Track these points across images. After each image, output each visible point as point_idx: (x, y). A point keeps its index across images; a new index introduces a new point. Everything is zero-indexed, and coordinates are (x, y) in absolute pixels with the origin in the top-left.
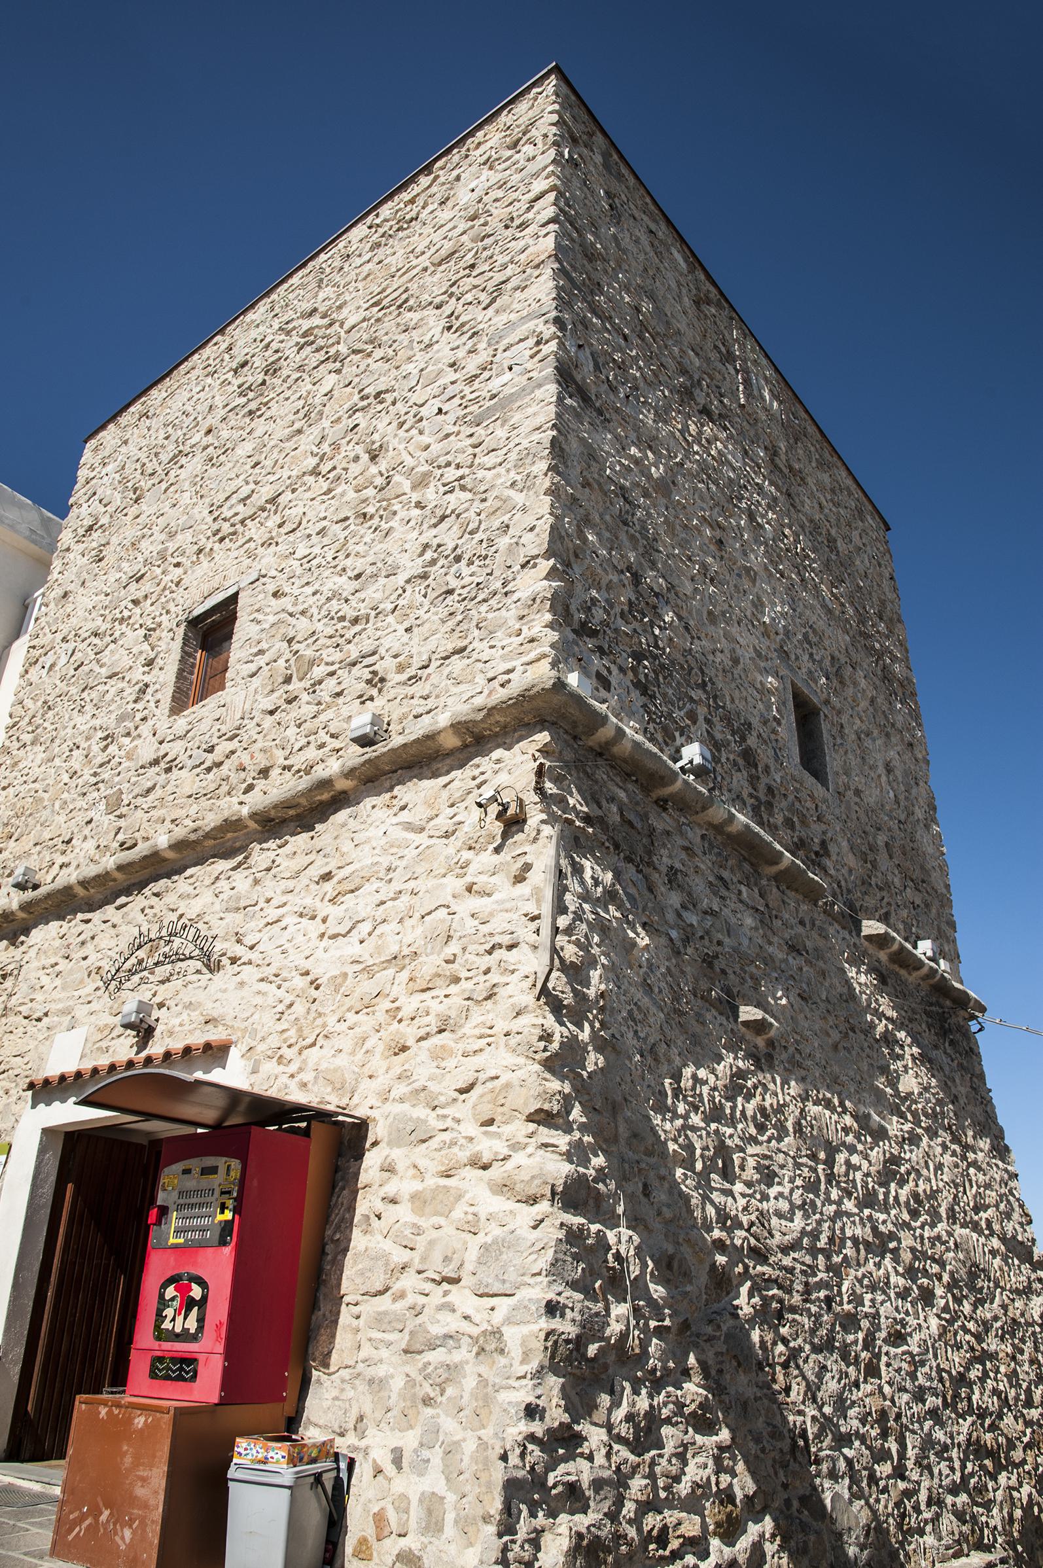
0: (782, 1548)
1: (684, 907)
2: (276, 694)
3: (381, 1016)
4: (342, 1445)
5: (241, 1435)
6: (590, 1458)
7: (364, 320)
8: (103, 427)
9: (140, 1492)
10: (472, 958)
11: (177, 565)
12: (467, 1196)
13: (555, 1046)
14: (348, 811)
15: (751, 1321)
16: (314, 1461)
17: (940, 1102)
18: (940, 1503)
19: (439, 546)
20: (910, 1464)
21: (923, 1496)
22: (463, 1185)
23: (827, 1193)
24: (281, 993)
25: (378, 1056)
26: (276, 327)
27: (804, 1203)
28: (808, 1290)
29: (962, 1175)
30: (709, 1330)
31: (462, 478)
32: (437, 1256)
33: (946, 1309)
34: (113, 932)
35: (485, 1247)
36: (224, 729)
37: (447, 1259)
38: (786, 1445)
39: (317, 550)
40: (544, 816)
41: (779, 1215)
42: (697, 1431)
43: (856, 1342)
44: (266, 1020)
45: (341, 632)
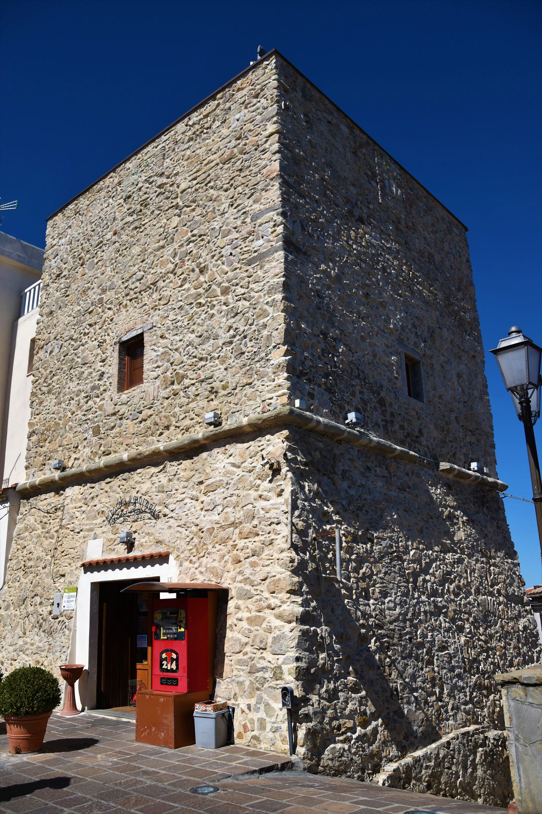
0: (385, 729)
1: (349, 487)
2: (168, 390)
3: (229, 547)
4: (230, 703)
5: (198, 702)
6: (313, 705)
7: (189, 188)
8: (56, 215)
9: (165, 721)
10: (263, 527)
11: (110, 309)
12: (267, 619)
13: (296, 564)
14: (207, 453)
15: (375, 652)
16: (221, 709)
17: (476, 540)
18: (458, 708)
19: (236, 329)
20: (445, 696)
21: (450, 707)
22: (265, 615)
23: (413, 595)
24: (187, 533)
25: (230, 563)
26: (144, 178)
27: (401, 602)
28: (401, 636)
29: (486, 571)
30: (358, 657)
31: (244, 294)
32: (258, 640)
33: (470, 632)
34: (106, 494)
35: (274, 638)
36: (146, 403)
37: (261, 642)
38: (388, 694)
39: (179, 318)
40: (288, 468)
41: (389, 609)
42: (352, 693)
43: (423, 653)
44: (182, 544)
45: (195, 364)
